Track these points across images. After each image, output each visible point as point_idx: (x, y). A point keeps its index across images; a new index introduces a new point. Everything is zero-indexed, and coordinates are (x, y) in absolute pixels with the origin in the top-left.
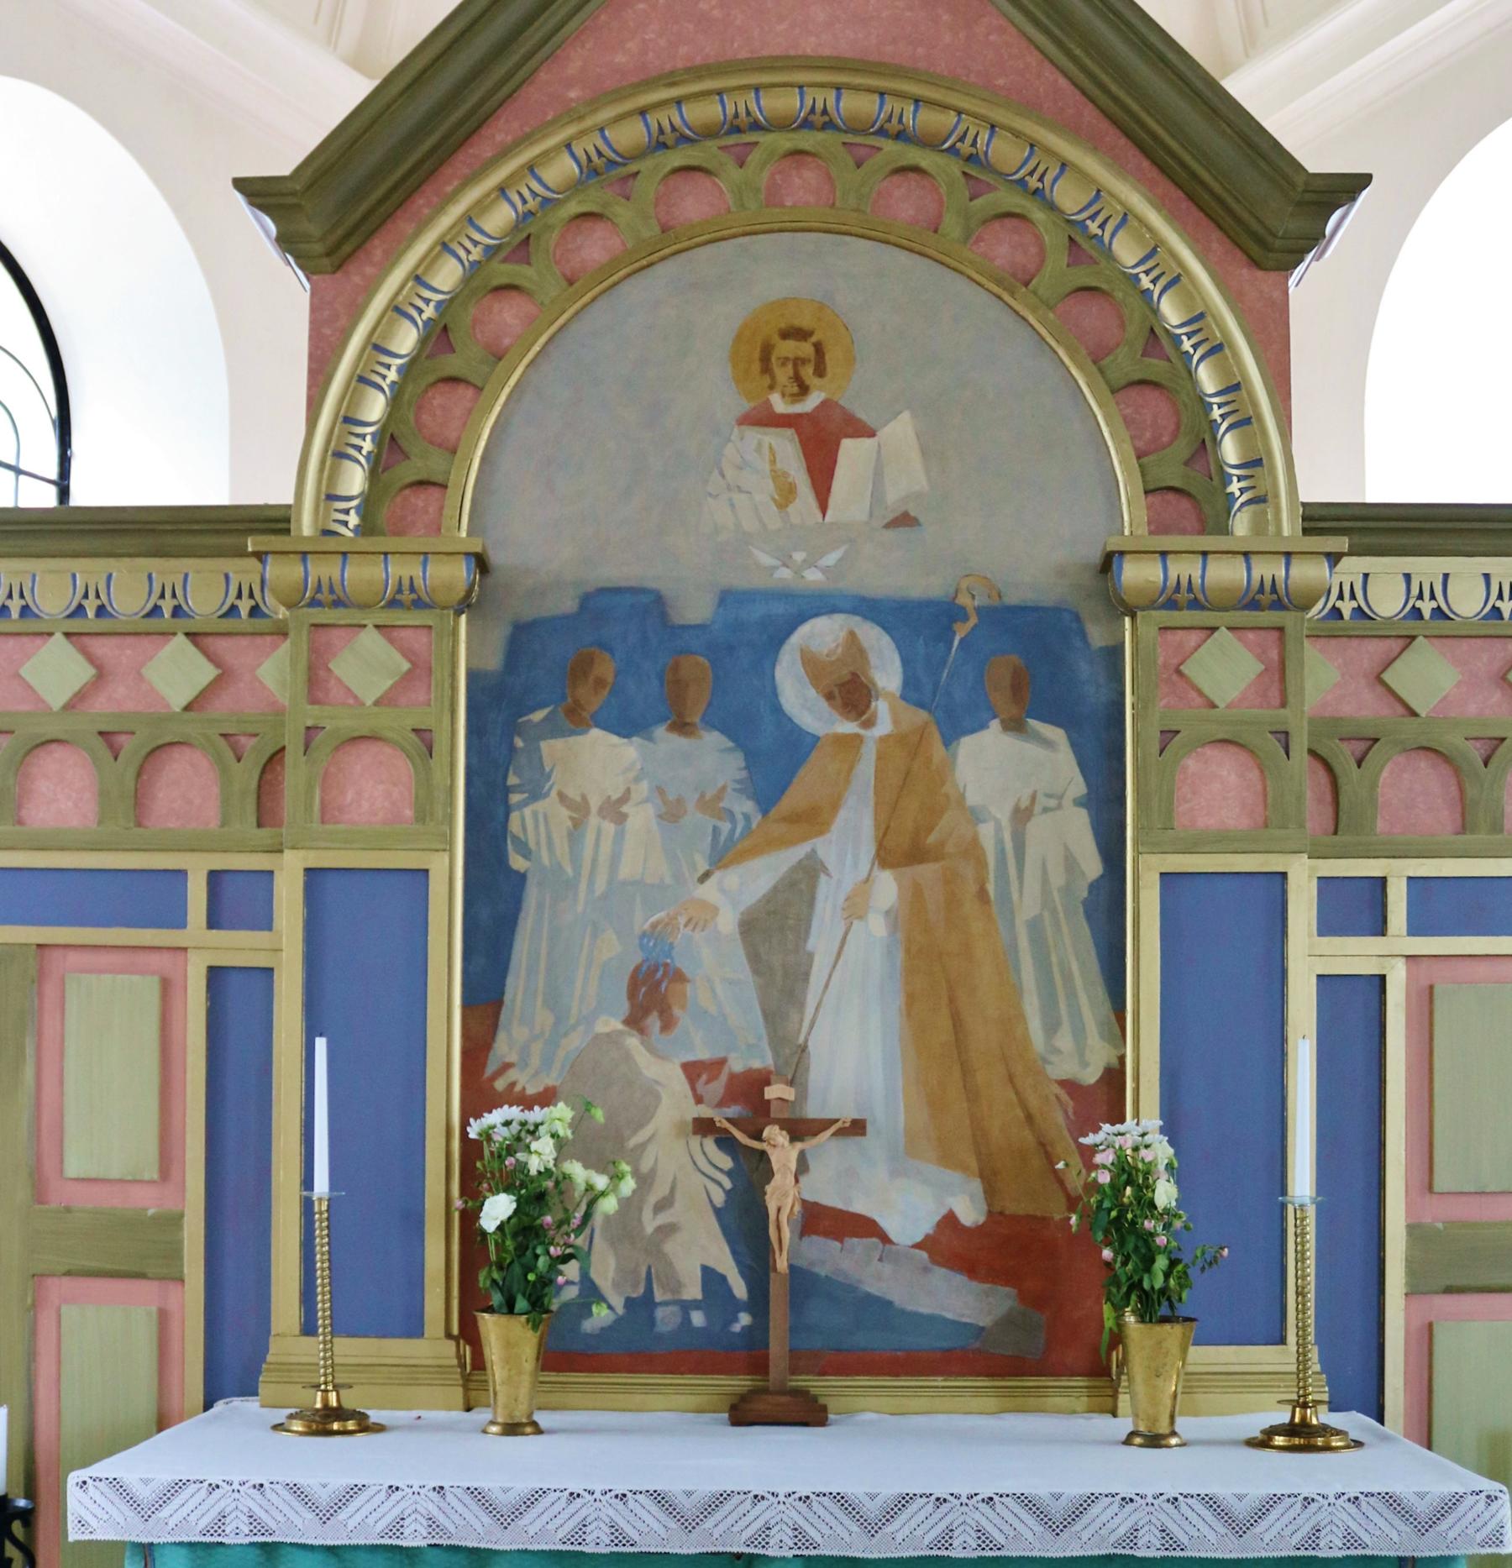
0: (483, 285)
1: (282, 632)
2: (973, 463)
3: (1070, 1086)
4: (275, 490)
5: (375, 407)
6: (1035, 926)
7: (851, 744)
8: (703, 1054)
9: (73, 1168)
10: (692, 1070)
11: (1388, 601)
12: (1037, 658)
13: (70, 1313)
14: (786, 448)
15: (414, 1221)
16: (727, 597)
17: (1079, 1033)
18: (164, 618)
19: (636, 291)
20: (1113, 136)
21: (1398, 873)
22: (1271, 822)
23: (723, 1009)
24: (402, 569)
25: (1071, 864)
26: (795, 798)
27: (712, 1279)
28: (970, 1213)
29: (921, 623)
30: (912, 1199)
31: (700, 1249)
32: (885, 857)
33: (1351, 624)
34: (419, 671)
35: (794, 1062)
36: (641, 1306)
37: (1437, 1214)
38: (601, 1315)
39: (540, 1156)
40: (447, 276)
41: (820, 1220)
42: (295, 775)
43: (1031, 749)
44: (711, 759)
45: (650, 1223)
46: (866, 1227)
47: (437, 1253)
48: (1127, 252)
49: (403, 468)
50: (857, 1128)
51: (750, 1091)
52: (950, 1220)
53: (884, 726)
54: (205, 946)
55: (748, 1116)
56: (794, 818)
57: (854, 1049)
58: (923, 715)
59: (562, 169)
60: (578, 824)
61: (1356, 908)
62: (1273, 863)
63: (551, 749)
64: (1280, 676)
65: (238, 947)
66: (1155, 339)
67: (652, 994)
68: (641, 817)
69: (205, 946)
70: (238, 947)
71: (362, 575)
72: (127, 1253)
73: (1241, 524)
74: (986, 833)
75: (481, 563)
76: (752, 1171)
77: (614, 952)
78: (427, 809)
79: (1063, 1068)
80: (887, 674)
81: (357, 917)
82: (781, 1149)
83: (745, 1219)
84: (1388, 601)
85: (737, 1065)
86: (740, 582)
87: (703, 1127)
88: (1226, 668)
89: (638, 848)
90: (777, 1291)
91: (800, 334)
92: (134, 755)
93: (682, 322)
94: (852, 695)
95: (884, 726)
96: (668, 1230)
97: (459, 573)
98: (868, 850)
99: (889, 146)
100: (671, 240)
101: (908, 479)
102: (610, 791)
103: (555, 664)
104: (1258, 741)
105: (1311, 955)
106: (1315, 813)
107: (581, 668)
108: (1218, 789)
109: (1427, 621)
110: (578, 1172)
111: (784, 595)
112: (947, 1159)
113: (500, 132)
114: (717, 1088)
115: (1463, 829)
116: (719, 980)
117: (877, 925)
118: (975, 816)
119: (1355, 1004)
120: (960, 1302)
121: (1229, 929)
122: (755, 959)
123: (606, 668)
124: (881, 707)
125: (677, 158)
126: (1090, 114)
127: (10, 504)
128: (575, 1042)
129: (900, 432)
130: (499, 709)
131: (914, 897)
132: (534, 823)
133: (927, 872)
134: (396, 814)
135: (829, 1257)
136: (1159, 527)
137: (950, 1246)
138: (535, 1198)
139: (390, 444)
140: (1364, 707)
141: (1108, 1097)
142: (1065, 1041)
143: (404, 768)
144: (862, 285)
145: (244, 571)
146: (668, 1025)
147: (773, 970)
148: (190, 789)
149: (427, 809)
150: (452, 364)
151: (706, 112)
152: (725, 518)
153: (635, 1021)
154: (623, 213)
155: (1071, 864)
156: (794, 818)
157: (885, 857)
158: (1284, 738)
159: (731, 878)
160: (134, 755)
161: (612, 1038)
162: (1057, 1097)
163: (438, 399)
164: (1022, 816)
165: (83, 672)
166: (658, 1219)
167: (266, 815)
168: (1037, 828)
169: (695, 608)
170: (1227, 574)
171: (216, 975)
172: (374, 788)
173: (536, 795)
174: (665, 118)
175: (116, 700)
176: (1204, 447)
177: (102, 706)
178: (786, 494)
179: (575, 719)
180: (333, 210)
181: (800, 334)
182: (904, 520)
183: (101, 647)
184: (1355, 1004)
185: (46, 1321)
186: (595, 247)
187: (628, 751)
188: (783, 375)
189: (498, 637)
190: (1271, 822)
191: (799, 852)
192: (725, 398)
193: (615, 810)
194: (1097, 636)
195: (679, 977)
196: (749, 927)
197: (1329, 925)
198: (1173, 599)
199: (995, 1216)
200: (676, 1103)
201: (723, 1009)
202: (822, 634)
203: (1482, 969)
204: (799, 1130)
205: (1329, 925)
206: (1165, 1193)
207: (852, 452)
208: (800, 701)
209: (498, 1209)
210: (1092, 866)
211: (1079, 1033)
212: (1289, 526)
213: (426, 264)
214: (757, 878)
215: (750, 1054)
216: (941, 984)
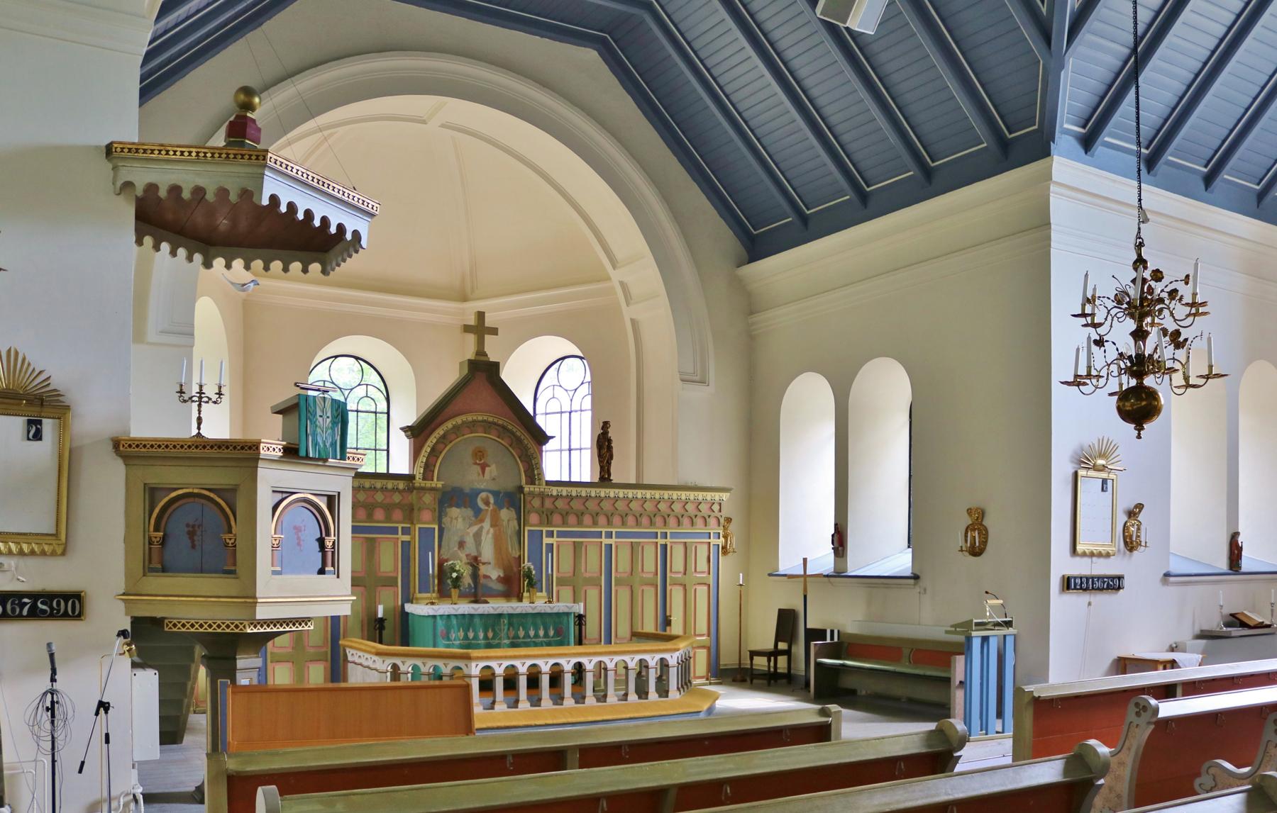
12: (513, 499)
14: (478, 468)
21: (555, 529)
23: (470, 548)
29: (496, 494)
32: (492, 526)
35: (480, 554)
44: (469, 512)
49: (428, 469)
51: (476, 559)
55: (475, 562)
57: (487, 553)
61: (550, 534)
67: (461, 544)
68: (460, 520)
70: (406, 538)
77: (456, 539)
80: (492, 501)
81: (426, 534)
89: (460, 524)
92: (389, 508)
94: (487, 503)
101: (495, 473)
102: (457, 517)
103: (452, 497)
104: (540, 513)
105: (546, 540)
108: (534, 518)
116: (470, 540)
129: (493, 467)
132: (445, 520)
137: (500, 580)
140: (552, 507)
152: (472, 478)
160: (389, 508)
162: (1173, 664)
169: (467, 491)
172: (427, 515)
179: (451, 506)
180: (417, 432)
190: (541, 524)
198: (530, 493)
201: (470, 548)
202: (483, 495)
208: (481, 504)
214: (475, 528)
215: (475, 554)
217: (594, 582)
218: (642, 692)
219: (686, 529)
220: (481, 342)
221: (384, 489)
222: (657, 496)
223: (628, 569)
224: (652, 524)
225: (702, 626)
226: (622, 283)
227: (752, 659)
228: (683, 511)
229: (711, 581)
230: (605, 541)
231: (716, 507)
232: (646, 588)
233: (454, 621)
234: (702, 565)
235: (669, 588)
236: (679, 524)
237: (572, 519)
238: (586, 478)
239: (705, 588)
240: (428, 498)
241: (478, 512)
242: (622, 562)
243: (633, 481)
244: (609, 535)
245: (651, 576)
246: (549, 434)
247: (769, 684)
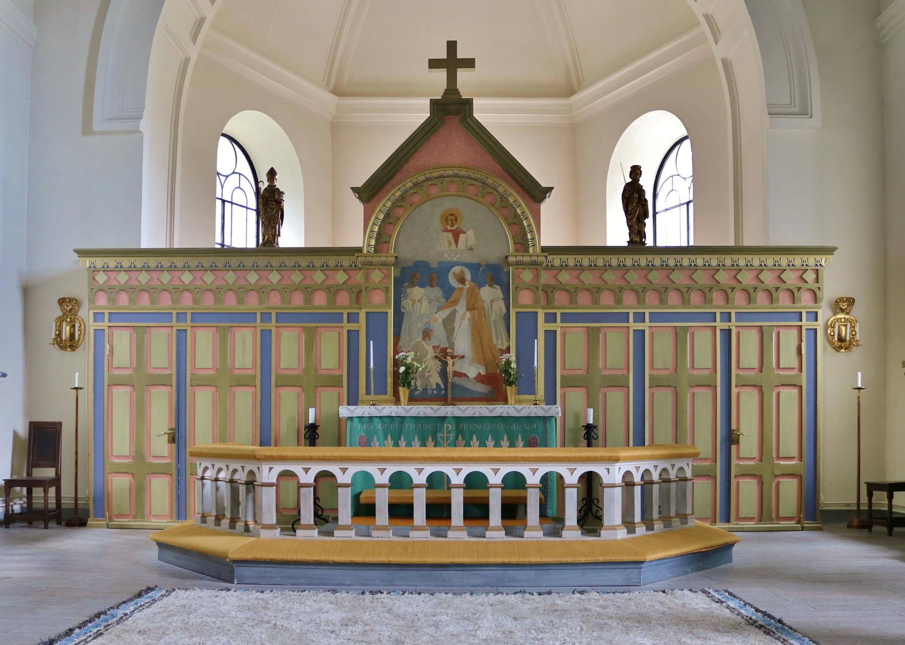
0: (394, 206)
1: (360, 269)
2: (482, 239)
3: (500, 350)
4: (359, 244)
5: (376, 229)
6: (494, 321)
7: (461, 289)
8: (436, 344)
9: (323, 366)
10: (434, 347)
11: (557, 263)
12: (494, 274)
13: (322, 394)
14: (450, 236)
15: (385, 374)
16: (440, 263)
17: (502, 340)
18: (338, 267)
19: (424, 206)
20: (509, 178)
22: (536, 302)
23: (439, 336)
24: (383, 259)
25: (501, 310)
26: (451, 299)
27: (437, 385)
28: (483, 372)
29: (474, 268)
30: (473, 370)
31: (436, 379)
32: (468, 309)
33: (550, 267)
34: (387, 276)
35: (452, 346)
36: (425, 390)
37: (565, 373)
38: (417, 393)
39: (409, 360)
40: (389, 204)
41: (456, 374)
42: (364, 295)
43: (494, 290)
44: (437, 292)
45: (427, 375)
46: (465, 375)
47: (390, 380)
48: (511, 200)
49: (382, 239)
50: (463, 357)
51: (444, 351)
52: (479, 374)
53: (468, 286)
54: (347, 326)
55: (443, 355)
56: (452, 302)
58: (474, 284)
59: (410, 184)
60: (413, 304)
62: (535, 310)
63: (409, 290)
64: (537, 276)
65: (353, 326)
66: (516, 215)
67: (427, 334)
68: (425, 302)
69: (347, 326)
70: (353, 326)
71: (376, 260)
72: (333, 382)
73: (531, 250)
74: (486, 305)
75: (396, 257)
76: (445, 364)
78: (387, 301)
79: (500, 347)
80: (468, 276)
81: (375, 321)
82: (450, 361)
83: (444, 374)
84: (557, 263)
85: (442, 346)
86: (442, 260)
87: (436, 357)
88: (527, 276)
89: (424, 308)
90: (449, 386)
91: (452, 215)
92: (333, 291)
93: (430, 213)
94: (462, 280)
95: (468, 286)
96: (430, 376)
97: (393, 259)
98: (465, 308)
99: (469, 180)
100: (429, 198)
101: (472, 241)
102: (420, 299)
103: (412, 274)
104: (533, 288)
106: (543, 301)
107: (414, 276)
108: (526, 297)
109: (564, 267)
110: (415, 363)
111: (450, 262)
112: (479, 363)
113: (398, 177)
114: (438, 350)
115: (571, 304)
117: (466, 322)
118: (484, 302)
119: (551, 336)
120: (481, 388)
121: (528, 323)
122: (445, 327)
123: (418, 276)
124: (467, 283)
125: (430, 183)
126: (505, 174)
127: (244, 246)
128: (413, 342)
129: (470, 233)
130: (399, 283)
131: (473, 316)
132: (406, 303)
133: (475, 312)
134: (381, 301)
135: (457, 380)
136: (517, 250)
137: (479, 379)
138: (408, 367)
139: (379, 235)
140: (552, 282)
141: (508, 350)
142: (500, 342)
143: (383, 294)
144: (464, 206)
145: (353, 258)
146: (430, 339)
147: (450, 331)
148: (344, 298)
149: (387, 301)
150: (390, 220)
151: (436, 174)
152: (439, 248)
153: (424, 339)
154: (421, 193)
155: (501, 310)
156: (452, 302)
157: (468, 309)
158: (537, 288)
159: (441, 313)
160: (333, 291)
161: (420, 342)
163: (388, 227)
164: (492, 302)
165: (323, 277)
166: (429, 373)
167: (357, 303)
168: (494, 304)
169: (434, 265)
170: (527, 259)
171: (349, 331)
172: (378, 298)
173: (406, 298)
174: (428, 175)
175: (330, 282)
176: (525, 235)
177: (327, 283)
178: (450, 244)
179: (413, 285)
180: (369, 192)
181: (452, 215)
182: (471, 249)
183: (327, 272)
184: (551, 336)
185: (318, 396)
186: (416, 199)
187: (422, 290)
188: (450, 222)
189: (399, 270)
191: (453, 308)
192: (439, 226)
193: (420, 301)
194: (505, 270)
195: (432, 331)
196: (444, 321)
197: (546, 321)
198: (518, 263)
199: (487, 373)
200: (431, 353)
201: (439, 336)
202: (457, 269)
203: (574, 329)
204: (453, 357)
205: (546, 321)
206: (513, 365)
207: (462, 236)
209: (402, 369)
210: (504, 311)
211: (502, 340)
212: (538, 251)
213: (385, 203)
214: (445, 313)
216: (478, 331)
217: (619, 383)
218: (553, 520)
219: (674, 304)
220: (452, 79)
221: (706, 267)
222: (714, 263)
223: (670, 364)
224: (707, 301)
225: (790, 443)
226: (194, 41)
227: (870, 495)
228: (755, 283)
229: (804, 380)
230: (633, 326)
231: (810, 276)
232: (697, 390)
233: (379, 426)
234: (789, 358)
235: (734, 391)
236: (750, 300)
237: (673, 297)
238: (252, 244)
239: (795, 392)
240: (376, 276)
241: (448, 292)
242: (660, 353)
243: (731, 243)
244: (640, 318)
245: (706, 373)
246: (544, 185)
247: (890, 533)
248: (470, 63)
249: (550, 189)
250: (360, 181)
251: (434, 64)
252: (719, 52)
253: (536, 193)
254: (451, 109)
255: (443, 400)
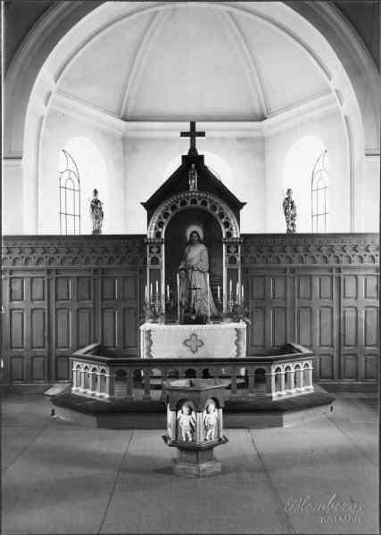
180: (151, 206)
220: (193, 143)
246: (242, 201)
248: (183, 134)
249: (245, 204)
250: (145, 199)
251: (202, 134)
252: (54, 87)
253: (236, 206)
254: (193, 161)
255: (68, 277)
